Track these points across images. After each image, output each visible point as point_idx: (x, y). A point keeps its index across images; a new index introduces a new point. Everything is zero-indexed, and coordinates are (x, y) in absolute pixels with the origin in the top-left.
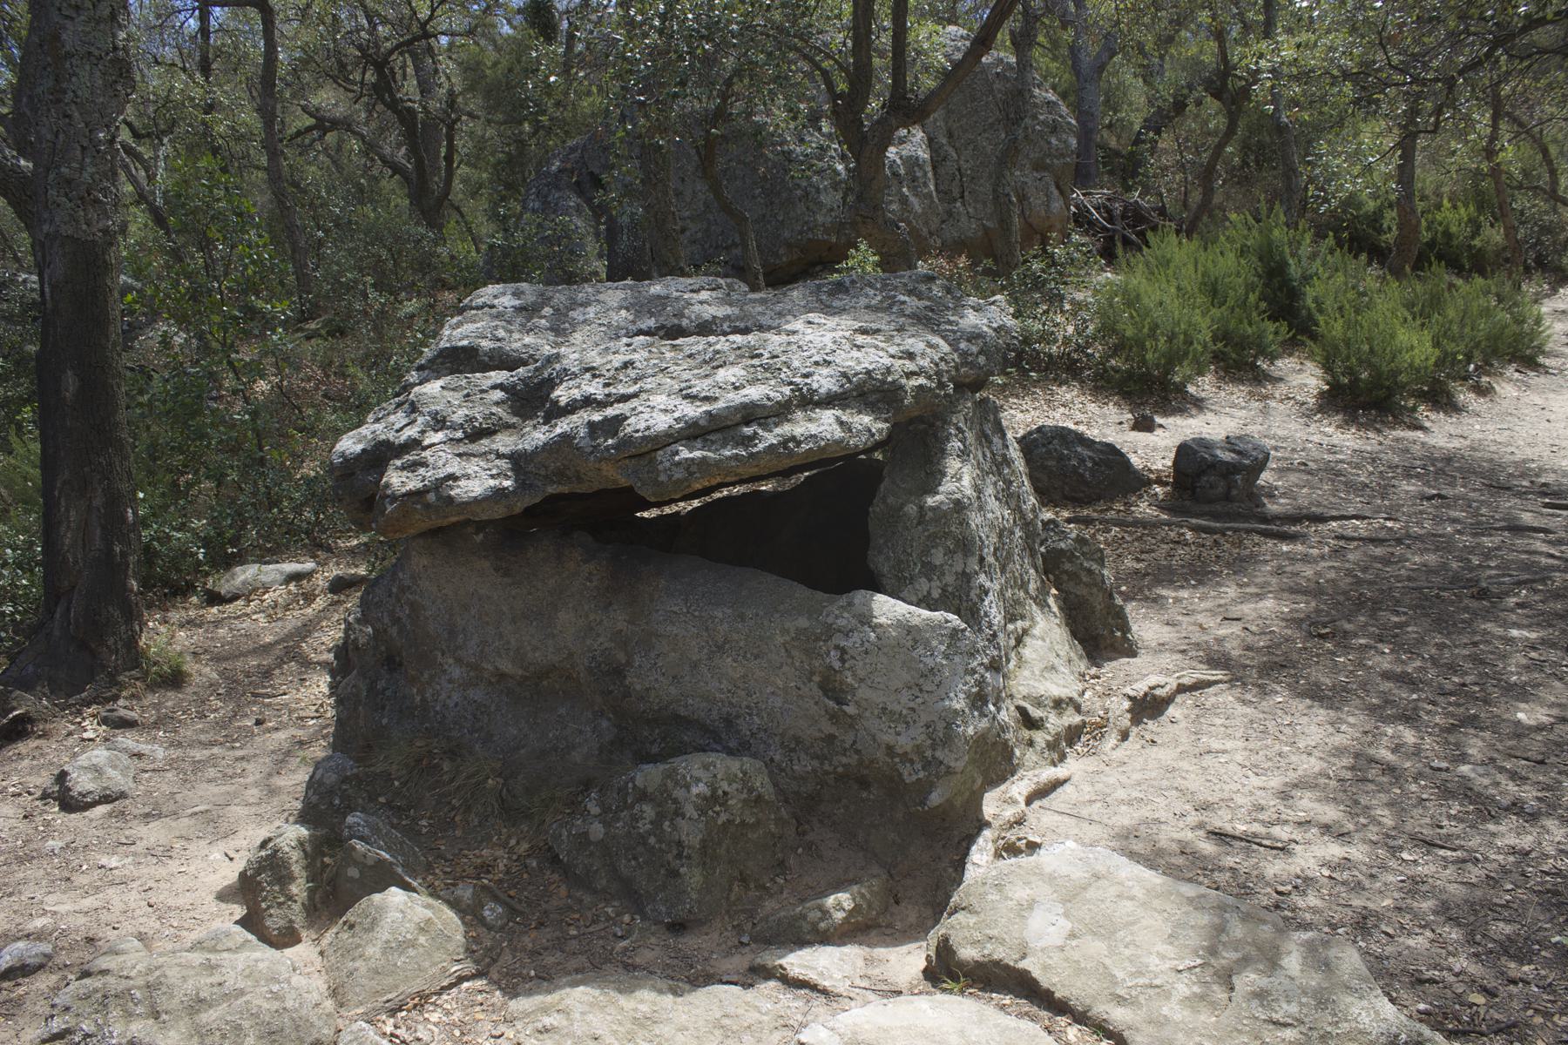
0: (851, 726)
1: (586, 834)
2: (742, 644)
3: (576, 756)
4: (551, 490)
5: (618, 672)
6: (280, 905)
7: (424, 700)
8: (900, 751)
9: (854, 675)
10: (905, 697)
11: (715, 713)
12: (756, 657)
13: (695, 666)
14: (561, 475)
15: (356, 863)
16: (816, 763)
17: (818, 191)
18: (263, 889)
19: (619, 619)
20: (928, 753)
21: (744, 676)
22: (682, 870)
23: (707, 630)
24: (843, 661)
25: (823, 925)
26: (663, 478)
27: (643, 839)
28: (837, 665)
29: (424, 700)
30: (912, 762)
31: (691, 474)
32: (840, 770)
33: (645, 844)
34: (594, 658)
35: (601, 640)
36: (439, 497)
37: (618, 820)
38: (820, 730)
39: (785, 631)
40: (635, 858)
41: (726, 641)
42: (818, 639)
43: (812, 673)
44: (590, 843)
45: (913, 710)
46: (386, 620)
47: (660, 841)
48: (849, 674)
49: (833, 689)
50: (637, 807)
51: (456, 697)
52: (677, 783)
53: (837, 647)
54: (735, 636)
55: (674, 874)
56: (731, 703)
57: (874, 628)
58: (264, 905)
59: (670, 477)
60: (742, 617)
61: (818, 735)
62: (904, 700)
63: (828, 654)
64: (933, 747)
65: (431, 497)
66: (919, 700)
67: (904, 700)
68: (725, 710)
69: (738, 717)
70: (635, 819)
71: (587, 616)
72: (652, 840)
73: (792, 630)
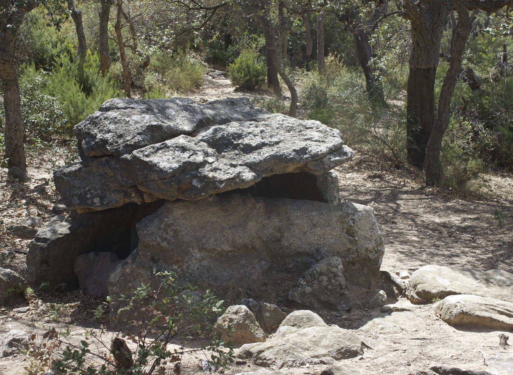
0: (356, 244)
1: (304, 292)
2: (323, 223)
3: (254, 277)
4: (264, 175)
5: (279, 240)
6: (257, 329)
10: (369, 232)
12: (328, 226)
13: (305, 233)
15: (268, 311)
16: (343, 259)
18: (249, 326)
19: (276, 221)
20: (376, 249)
21: (324, 234)
22: (345, 292)
23: (310, 220)
24: (354, 223)
27: (326, 288)
28: (353, 225)
30: (372, 252)
32: (351, 260)
33: (327, 289)
35: (269, 230)
36: (240, 180)
37: (314, 284)
38: (347, 247)
42: (345, 217)
43: (343, 229)
44: (306, 294)
45: (371, 236)
46: (159, 240)
47: (332, 286)
48: (356, 227)
49: (350, 233)
50: (320, 278)
51: (197, 266)
52: (332, 267)
53: (352, 219)
54: (321, 220)
55: (343, 294)
56: (318, 244)
57: (360, 212)
58: (252, 331)
60: (322, 214)
61: (345, 249)
62: (369, 233)
63: (349, 222)
67: (369, 233)
68: (316, 246)
69: (320, 248)
70: (320, 282)
71: (262, 223)
72: (330, 287)
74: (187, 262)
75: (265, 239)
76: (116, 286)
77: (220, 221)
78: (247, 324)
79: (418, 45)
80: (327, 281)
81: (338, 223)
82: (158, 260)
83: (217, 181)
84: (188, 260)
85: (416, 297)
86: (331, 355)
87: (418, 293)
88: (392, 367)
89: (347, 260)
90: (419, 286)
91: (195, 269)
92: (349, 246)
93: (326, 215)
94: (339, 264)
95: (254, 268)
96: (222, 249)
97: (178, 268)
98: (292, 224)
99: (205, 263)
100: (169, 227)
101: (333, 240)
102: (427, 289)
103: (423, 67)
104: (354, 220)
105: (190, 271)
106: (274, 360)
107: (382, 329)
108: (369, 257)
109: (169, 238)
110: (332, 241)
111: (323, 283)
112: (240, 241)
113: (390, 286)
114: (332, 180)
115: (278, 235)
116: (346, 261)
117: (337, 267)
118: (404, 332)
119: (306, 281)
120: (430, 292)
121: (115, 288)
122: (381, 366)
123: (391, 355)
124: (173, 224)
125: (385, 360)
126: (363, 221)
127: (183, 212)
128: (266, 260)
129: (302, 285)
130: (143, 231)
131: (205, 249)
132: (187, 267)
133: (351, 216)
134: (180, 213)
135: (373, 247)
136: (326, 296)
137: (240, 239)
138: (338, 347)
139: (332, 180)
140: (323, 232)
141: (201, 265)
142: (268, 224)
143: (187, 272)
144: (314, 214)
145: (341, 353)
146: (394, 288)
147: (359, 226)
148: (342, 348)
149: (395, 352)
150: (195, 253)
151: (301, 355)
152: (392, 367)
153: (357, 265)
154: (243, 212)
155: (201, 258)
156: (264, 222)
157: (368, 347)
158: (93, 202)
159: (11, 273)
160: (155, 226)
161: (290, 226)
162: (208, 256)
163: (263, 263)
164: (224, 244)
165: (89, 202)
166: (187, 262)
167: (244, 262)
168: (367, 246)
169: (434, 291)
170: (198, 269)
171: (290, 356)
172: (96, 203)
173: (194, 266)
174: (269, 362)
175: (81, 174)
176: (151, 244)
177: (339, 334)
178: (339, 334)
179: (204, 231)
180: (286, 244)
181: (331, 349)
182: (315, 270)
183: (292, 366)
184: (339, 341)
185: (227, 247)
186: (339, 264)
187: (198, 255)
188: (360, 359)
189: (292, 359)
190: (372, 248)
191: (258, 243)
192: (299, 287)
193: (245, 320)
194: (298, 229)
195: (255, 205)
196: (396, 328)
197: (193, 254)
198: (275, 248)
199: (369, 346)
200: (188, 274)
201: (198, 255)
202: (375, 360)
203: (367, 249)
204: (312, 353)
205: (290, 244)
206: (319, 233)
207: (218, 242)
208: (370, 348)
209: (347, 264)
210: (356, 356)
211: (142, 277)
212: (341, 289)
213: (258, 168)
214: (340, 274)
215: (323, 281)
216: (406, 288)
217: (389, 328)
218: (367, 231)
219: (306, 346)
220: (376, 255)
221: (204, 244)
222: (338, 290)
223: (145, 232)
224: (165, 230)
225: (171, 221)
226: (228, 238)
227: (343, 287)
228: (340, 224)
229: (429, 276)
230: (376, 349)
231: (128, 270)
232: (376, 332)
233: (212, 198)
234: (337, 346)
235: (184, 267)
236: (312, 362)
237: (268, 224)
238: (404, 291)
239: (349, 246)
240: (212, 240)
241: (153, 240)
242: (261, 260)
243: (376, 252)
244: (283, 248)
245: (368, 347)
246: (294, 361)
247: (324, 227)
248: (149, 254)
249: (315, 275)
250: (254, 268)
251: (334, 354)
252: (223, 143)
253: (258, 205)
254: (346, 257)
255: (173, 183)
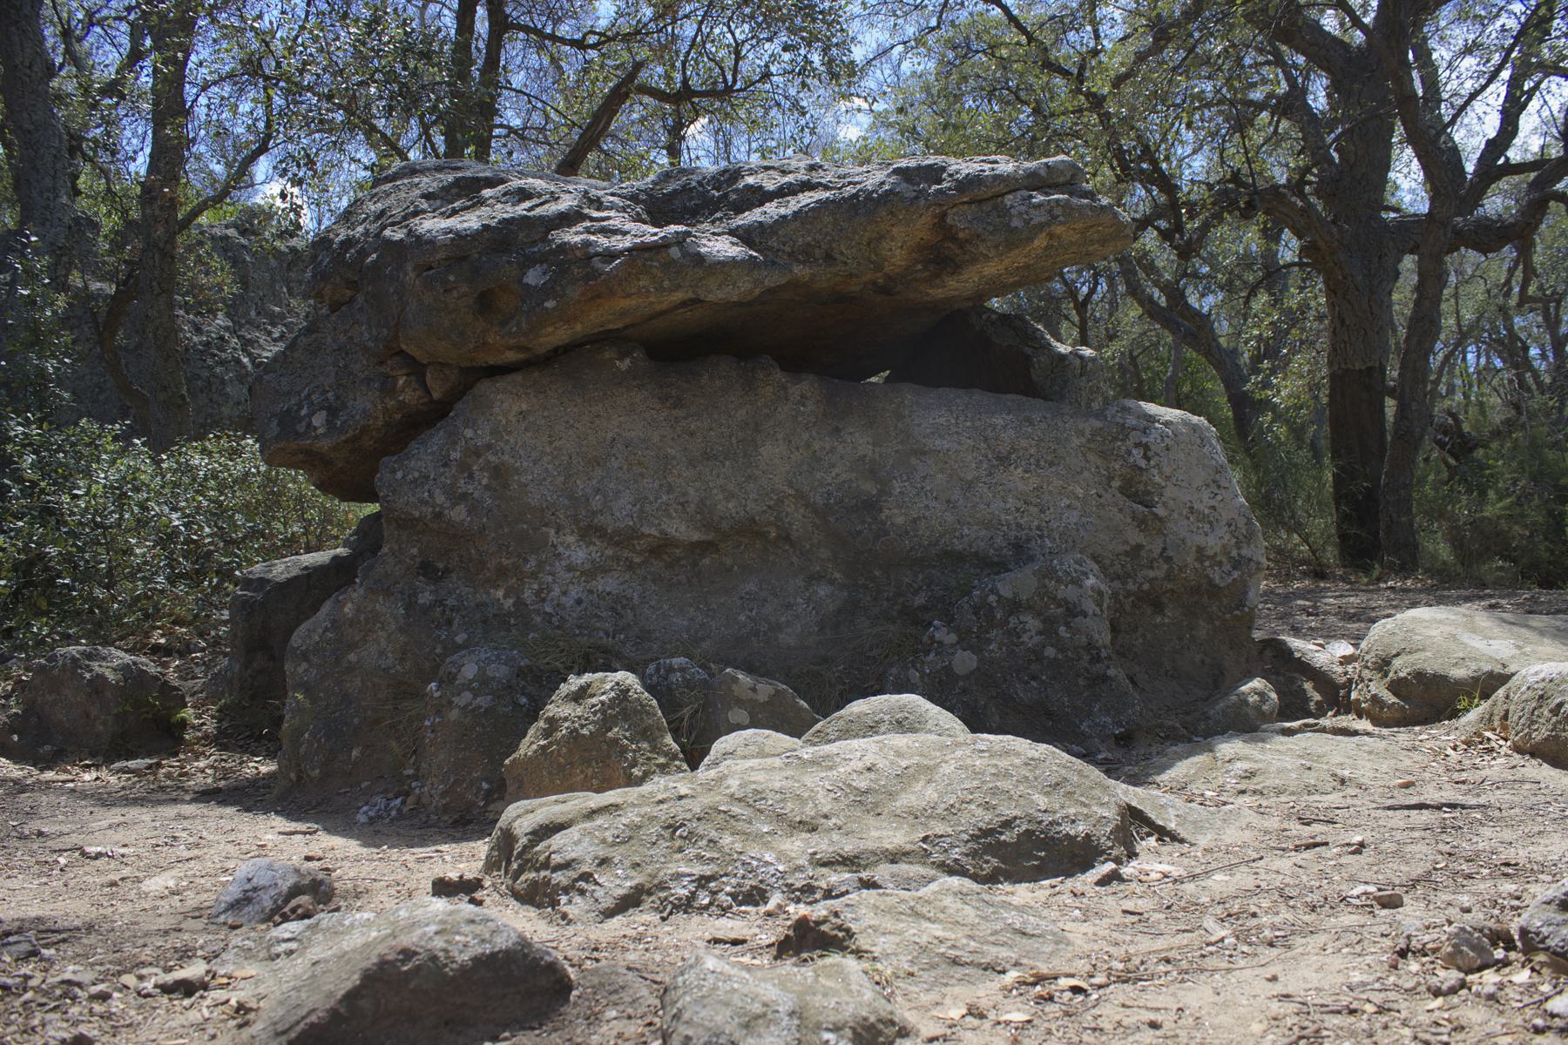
0: (1160, 532)
1: (948, 670)
4: (800, 271)
5: (870, 506)
7: (520, 603)
8: (1210, 553)
9: (1160, 473)
10: (1205, 495)
11: (999, 540)
12: (1051, 464)
13: (969, 486)
14: (805, 254)
15: (740, 702)
16: (1117, 584)
17: (223, 382)
18: (625, 750)
19: (859, 442)
20: (1234, 553)
22: (1111, 672)
23: (986, 439)
24: (1146, 457)
25: (1265, 708)
26: (1016, 223)
27: (1037, 654)
28: (1143, 463)
29: (520, 603)
30: (1220, 564)
31: (1055, 217)
32: (1146, 587)
34: (829, 494)
36: (685, 254)
37: (989, 641)
39: (1081, 433)
40: (1034, 678)
41: (1014, 450)
42: (1115, 439)
43: (1110, 478)
45: (1213, 508)
46: (440, 498)
47: (1062, 650)
48: (1155, 471)
49: (1137, 491)
50: (1013, 621)
51: (575, 592)
52: (1059, 581)
54: (1024, 443)
55: (1105, 679)
56: (1019, 526)
59: (1027, 222)
61: (1121, 548)
63: (1129, 453)
64: (1238, 546)
65: (675, 252)
66: (1219, 498)
69: (1028, 540)
70: (1014, 634)
71: (808, 446)
72: (1050, 652)
73: (1087, 432)
74: (534, 575)
75: (820, 501)
76: (306, 659)
77: (656, 439)
78: (616, 741)
79: (1343, 322)
80: (1039, 633)
81: (1091, 457)
82: (447, 571)
83: (597, 254)
84: (540, 564)
85: (1390, 698)
86: (937, 857)
87: (1396, 687)
88: (1285, 914)
89: (1131, 586)
90: (1397, 663)
91: (568, 602)
92: (1135, 536)
93: (1043, 425)
94: (1085, 574)
95: (789, 606)
96: (662, 532)
97: (505, 597)
98: (921, 453)
99: (607, 584)
100: (479, 456)
101: (1075, 513)
102: (1431, 667)
103: (1358, 366)
104: (1146, 447)
105: (548, 609)
106: (585, 868)
107: (1250, 775)
108: (1210, 581)
109: (476, 495)
110: (1073, 517)
111: (1025, 638)
112: (729, 508)
113: (1292, 680)
114: (1083, 367)
115: (870, 488)
116: (1128, 594)
117: (1077, 582)
118: (1351, 791)
119: (957, 630)
120: (1444, 678)
121: (305, 665)
122: (1219, 910)
123: (1285, 864)
124: (489, 447)
125: (1249, 882)
126: (1182, 455)
127: (524, 407)
128: (832, 582)
129: (940, 643)
130: (394, 471)
131: (601, 532)
132: (538, 593)
133: (1135, 437)
134: (515, 408)
135: (1224, 546)
136: (1034, 683)
137: (727, 499)
138: (984, 818)
139: (1083, 367)
140: (1034, 482)
141: (591, 592)
142: (833, 450)
143: (538, 612)
144: (998, 421)
145: (998, 849)
146: (1308, 686)
147: (1167, 470)
148: (1008, 824)
149: (1308, 855)
150: (568, 547)
151: (754, 851)
152: (1285, 914)
153: (1171, 613)
154: (743, 412)
155: (587, 566)
156: (816, 446)
157: (1163, 834)
158: (309, 425)
159: (135, 663)
160: (433, 453)
161: (914, 461)
162: (617, 559)
163: (823, 590)
164: (671, 517)
165: (301, 428)
166: (534, 575)
167: (751, 587)
168: (1199, 540)
169: (1459, 673)
170: (579, 602)
171: (691, 851)
172: (315, 429)
173: (564, 593)
174: (559, 878)
175: (296, 355)
176: (417, 514)
177: (1003, 763)
178: (1003, 763)
179: (599, 472)
180: (900, 520)
181: (939, 828)
182: (993, 591)
183: (686, 905)
184: (995, 791)
185: (683, 528)
186: (1085, 574)
187: (580, 555)
188: (1104, 881)
189: (698, 870)
190: (1218, 549)
191: (797, 519)
192: (927, 653)
193: (606, 723)
194: (942, 471)
195: (785, 388)
196: (1313, 774)
197: (561, 549)
198: (859, 533)
199: (1172, 826)
200: (539, 619)
201: (580, 555)
202: (1189, 887)
203: (1200, 550)
204: (823, 845)
205: (915, 521)
206: (1021, 486)
207: (648, 508)
208: (1175, 838)
209: (1134, 605)
210: (1086, 866)
211: (383, 629)
212: (1096, 659)
213: (773, 242)
214: (1090, 606)
215: (1025, 631)
216: (1350, 681)
217: (1279, 771)
218: (1198, 489)
219: (809, 811)
220: (1236, 574)
221: (594, 513)
222: (1084, 663)
223: (399, 475)
224: (464, 467)
225: (483, 436)
226: (685, 494)
227: (1104, 654)
228: (1099, 461)
229: (1434, 633)
230: (1204, 841)
231: (348, 609)
232: (1222, 789)
233: (627, 362)
234: (979, 812)
235: (527, 595)
236: (809, 889)
237: (833, 450)
238: (1342, 692)
239: (1135, 536)
240: (625, 499)
241: (423, 502)
242: (813, 578)
243: (1237, 564)
244: (886, 533)
245: (1163, 834)
246: (703, 881)
247: (1038, 465)
248: (415, 551)
249: (991, 608)
250: (789, 606)
251: (955, 853)
252: (685, 207)
253: (795, 391)
254: (1129, 576)
255: (452, 278)
